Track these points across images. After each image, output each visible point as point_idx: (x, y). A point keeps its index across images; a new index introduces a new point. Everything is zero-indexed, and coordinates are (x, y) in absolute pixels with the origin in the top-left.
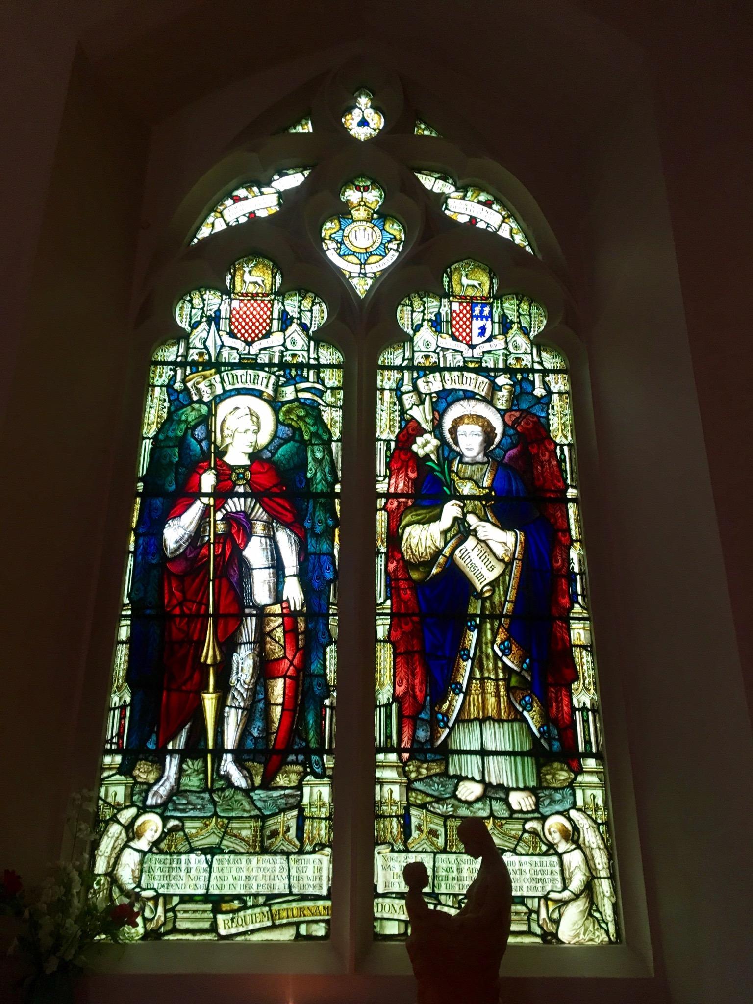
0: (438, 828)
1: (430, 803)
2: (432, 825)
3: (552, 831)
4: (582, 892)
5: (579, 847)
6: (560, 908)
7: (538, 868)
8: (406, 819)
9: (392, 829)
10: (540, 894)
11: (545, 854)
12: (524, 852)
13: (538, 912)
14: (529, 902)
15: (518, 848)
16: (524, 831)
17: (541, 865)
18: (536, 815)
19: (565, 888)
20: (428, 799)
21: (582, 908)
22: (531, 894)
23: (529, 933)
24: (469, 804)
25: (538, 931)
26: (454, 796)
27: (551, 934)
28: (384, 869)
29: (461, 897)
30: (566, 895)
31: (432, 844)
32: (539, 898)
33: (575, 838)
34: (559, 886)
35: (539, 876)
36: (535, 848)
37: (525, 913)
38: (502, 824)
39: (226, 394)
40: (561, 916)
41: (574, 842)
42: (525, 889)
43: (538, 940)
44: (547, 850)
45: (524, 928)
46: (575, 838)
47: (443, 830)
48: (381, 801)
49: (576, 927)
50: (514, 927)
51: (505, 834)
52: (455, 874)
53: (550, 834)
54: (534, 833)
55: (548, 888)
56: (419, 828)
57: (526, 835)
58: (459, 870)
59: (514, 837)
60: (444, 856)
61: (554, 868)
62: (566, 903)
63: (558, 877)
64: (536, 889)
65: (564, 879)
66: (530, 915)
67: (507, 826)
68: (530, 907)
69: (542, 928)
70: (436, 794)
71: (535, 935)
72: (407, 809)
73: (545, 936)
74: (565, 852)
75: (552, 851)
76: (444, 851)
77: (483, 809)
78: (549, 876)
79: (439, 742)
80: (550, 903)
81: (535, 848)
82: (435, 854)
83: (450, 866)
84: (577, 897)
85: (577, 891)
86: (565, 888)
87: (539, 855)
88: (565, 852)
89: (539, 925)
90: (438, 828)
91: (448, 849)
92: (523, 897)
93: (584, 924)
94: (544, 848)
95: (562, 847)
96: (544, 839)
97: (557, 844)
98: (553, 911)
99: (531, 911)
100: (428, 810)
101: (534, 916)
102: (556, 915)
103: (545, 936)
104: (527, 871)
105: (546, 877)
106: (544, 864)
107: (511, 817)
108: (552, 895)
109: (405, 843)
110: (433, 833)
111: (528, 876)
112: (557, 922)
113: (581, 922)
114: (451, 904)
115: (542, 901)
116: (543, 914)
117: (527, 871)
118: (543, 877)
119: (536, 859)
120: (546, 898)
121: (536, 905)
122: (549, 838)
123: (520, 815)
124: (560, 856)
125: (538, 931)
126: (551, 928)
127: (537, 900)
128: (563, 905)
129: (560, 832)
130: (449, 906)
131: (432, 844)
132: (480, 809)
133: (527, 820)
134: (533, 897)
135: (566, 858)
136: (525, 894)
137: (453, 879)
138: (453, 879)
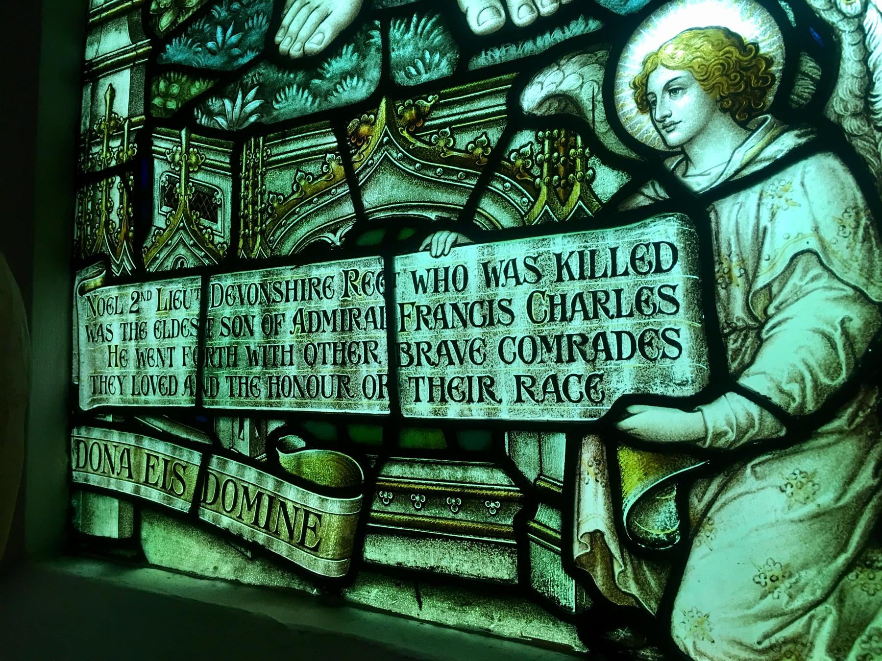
0: (217, 181)
1: (200, 100)
2: (200, 177)
3: (657, 83)
4: (832, 403)
5: (825, 137)
6: (684, 487)
7: (572, 288)
8: (138, 169)
9: (109, 210)
10: (573, 413)
11: (616, 213)
12: (506, 220)
13: (566, 501)
14: (526, 453)
15: (488, 206)
16: (515, 120)
17: (588, 272)
18: (577, 28)
19: (720, 380)
20: (196, 88)
21: (826, 499)
22: (530, 412)
23: (521, 594)
24: (311, 64)
25: (566, 591)
26: (270, 53)
27: (633, 615)
28: (91, 337)
29: (274, 426)
30: (727, 415)
31: (201, 241)
32: (574, 433)
33: (804, 89)
34: (685, 369)
35: (577, 325)
36: (559, 193)
37: (506, 501)
38: (422, 115)
39: (845, 16)
40: (690, 527)
41: (787, 116)
42: (505, 390)
43: (562, 635)
44: (625, 193)
45: (499, 568)
46: (804, 89)
47: (227, 185)
48: (91, 130)
49: (780, 599)
50: (375, 508)
51: (430, 156)
52: (257, 340)
53: (646, 103)
54: (565, 117)
55: (623, 379)
56: (170, 198)
57: (524, 139)
58: (271, 325)
59: (467, 161)
60: (227, 281)
61: (656, 280)
62: (721, 462)
63: (683, 324)
64: (558, 389)
65: (713, 334)
66: (528, 513)
67: (443, 116)
68: (531, 475)
69: (583, 581)
70: (215, 61)
71: (551, 609)
72: (144, 139)
73: (598, 617)
74: (734, 185)
75: (653, 192)
76: (231, 262)
77: (357, 72)
78: (577, 287)
79: (434, 19)
80: (627, 458)
81: (559, 193)
82: (205, 273)
83: (243, 310)
84: (793, 430)
85: (801, 397)
86: (720, 380)
87: (577, 224)
88: (734, 185)
89: (572, 567)
90: (217, 181)
91: (242, 253)
92: (496, 429)
93: (836, 589)
94: (607, 182)
95: (715, 157)
96: (611, 142)
97: (682, 152)
98: (648, 500)
99: (532, 495)
100: (195, 128)
101: (547, 518)
102: (661, 523)
103: (598, 617)
104: (519, 307)
105: (612, 325)
106: (604, 261)
107: (461, 74)
108: (644, 420)
109: (137, 256)
110: (204, 203)
111: (521, 327)
112: (669, 561)
113: (815, 581)
114: (244, 448)
115: (589, 451)
116: (593, 511)
117: (519, 307)
118: (590, 329)
119: (562, 244)
120: (609, 432)
121: (557, 465)
122: (642, 127)
123: (498, 55)
124: (696, 210)
125: (566, 591)
126: (630, 583)
127: (560, 441)
128: (707, 474)
129: (705, 80)
130: (239, 458)
131: (201, 241)
132: (345, 75)
133: (528, 69)
134: (541, 430)
135: (733, 217)
136: (505, 414)
137: (253, 358)
138: (253, 358)
